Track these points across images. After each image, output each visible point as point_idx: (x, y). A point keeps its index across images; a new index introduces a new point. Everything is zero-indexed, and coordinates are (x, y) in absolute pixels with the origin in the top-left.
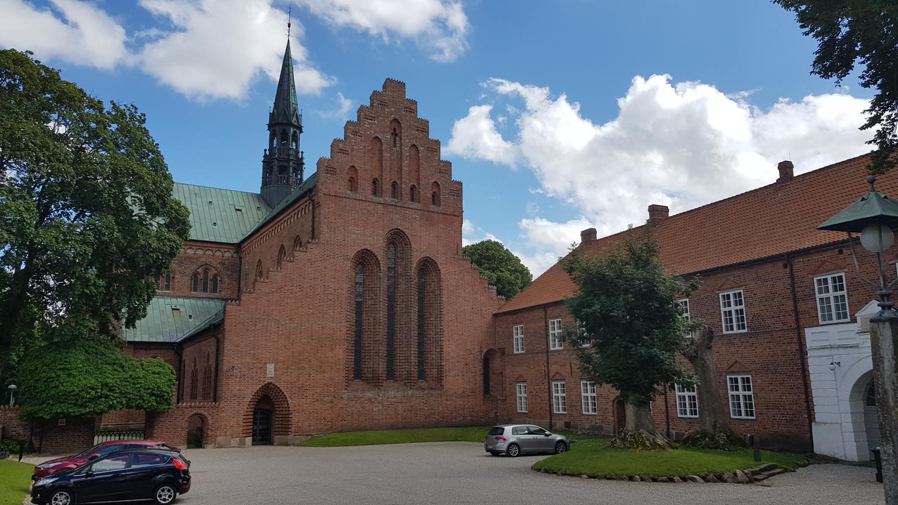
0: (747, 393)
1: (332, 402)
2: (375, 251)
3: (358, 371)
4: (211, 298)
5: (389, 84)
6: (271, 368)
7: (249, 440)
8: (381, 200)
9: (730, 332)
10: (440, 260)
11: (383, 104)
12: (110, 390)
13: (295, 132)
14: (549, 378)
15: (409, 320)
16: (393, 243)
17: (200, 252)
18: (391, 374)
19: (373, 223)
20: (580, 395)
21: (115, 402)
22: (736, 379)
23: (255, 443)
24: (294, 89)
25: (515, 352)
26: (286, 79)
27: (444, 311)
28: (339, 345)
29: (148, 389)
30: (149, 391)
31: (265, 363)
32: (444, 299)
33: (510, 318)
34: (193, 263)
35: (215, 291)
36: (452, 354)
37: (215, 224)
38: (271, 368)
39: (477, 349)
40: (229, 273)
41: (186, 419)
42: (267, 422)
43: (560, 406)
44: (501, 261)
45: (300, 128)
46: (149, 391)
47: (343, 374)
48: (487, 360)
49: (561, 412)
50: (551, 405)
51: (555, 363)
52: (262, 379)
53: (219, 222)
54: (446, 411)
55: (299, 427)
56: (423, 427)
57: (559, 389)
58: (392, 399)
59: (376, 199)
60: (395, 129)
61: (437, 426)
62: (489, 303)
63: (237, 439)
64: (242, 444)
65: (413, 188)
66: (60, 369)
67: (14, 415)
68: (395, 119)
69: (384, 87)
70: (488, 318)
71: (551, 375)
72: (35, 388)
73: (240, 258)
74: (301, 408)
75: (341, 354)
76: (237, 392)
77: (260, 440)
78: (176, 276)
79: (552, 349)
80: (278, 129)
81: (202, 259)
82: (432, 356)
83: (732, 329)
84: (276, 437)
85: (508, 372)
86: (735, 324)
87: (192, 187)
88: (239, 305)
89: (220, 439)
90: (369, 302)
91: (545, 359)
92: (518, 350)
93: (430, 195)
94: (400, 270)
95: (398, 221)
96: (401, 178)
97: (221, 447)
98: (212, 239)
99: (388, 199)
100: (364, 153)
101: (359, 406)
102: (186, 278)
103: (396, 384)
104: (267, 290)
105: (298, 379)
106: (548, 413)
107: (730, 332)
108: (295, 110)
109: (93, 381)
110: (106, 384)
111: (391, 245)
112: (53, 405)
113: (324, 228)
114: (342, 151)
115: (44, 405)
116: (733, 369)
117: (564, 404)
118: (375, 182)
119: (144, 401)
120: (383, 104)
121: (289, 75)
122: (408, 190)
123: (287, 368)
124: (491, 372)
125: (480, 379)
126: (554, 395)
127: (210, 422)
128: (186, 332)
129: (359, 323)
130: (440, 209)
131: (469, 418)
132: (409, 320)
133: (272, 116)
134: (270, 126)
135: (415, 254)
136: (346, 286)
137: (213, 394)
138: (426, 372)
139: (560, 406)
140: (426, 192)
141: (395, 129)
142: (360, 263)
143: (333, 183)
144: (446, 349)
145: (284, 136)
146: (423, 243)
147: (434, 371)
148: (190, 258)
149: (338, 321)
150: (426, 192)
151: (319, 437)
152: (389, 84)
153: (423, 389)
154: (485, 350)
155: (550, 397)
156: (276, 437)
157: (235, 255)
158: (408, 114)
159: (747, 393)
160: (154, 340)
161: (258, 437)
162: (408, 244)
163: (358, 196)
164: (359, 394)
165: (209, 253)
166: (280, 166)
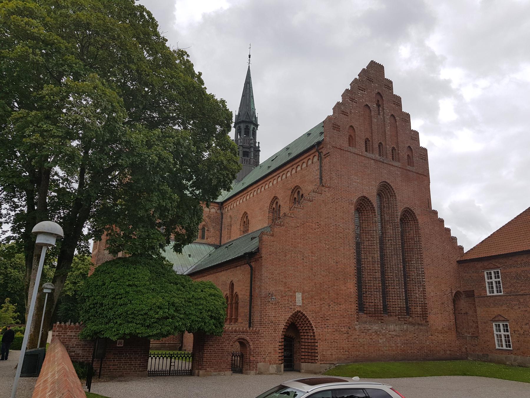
0: (506, 333)
4: (201, 243)
5: (373, 64)
9: (492, 294)
10: (417, 212)
11: (370, 80)
12: (176, 310)
13: (254, 128)
15: (395, 262)
21: (180, 323)
22: (499, 325)
24: (253, 99)
26: (248, 92)
27: (424, 256)
30: (210, 313)
31: (295, 292)
33: (479, 265)
35: (203, 237)
36: (432, 294)
39: (449, 290)
40: (214, 224)
42: (296, 347)
45: (257, 126)
52: (293, 307)
55: (323, 356)
58: (390, 334)
60: (378, 101)
61: (426, 359)
63: (275, 366)
66: (129, 285)
67: (73, 334)
68: (379, 93)
72: (102, 304)
73: (222, 214)
76: (273, 319)
80: (243, 126)
82: (417, 294)
83: (493, 293)
84: (303, 365)
86: (495, 289)
89: (260, 365)
90: (366, 243)
94: (387, 218)
97: (260, 373)
100: (359, 116)
103: (391, 319)
107: (492, 294)
108: (254, 113)
109: (161, 300)
110: (173, 304)
112: (120, 324)
115: (111, 324)
116: (497, 319)
119: (205, 323)
121: (250, 89)
123: (312, 297)
128: (189, 267)
129: (359, 261)
131: (448, 352)
132: (395, 262)
135: (399, 204)
138: (412, 311)
140: (403, 154)
141: (378, 101)
145: (247, 133)
146: (404, 196)
147: (419, 309)
150: (403, 154)
152: (373, 64)
156: (303, 365)
157: (219, 212)
158: (387, 90)
159: (506, 333)
162: (394, 195)
164: (368, 326)
166: (244, 152)
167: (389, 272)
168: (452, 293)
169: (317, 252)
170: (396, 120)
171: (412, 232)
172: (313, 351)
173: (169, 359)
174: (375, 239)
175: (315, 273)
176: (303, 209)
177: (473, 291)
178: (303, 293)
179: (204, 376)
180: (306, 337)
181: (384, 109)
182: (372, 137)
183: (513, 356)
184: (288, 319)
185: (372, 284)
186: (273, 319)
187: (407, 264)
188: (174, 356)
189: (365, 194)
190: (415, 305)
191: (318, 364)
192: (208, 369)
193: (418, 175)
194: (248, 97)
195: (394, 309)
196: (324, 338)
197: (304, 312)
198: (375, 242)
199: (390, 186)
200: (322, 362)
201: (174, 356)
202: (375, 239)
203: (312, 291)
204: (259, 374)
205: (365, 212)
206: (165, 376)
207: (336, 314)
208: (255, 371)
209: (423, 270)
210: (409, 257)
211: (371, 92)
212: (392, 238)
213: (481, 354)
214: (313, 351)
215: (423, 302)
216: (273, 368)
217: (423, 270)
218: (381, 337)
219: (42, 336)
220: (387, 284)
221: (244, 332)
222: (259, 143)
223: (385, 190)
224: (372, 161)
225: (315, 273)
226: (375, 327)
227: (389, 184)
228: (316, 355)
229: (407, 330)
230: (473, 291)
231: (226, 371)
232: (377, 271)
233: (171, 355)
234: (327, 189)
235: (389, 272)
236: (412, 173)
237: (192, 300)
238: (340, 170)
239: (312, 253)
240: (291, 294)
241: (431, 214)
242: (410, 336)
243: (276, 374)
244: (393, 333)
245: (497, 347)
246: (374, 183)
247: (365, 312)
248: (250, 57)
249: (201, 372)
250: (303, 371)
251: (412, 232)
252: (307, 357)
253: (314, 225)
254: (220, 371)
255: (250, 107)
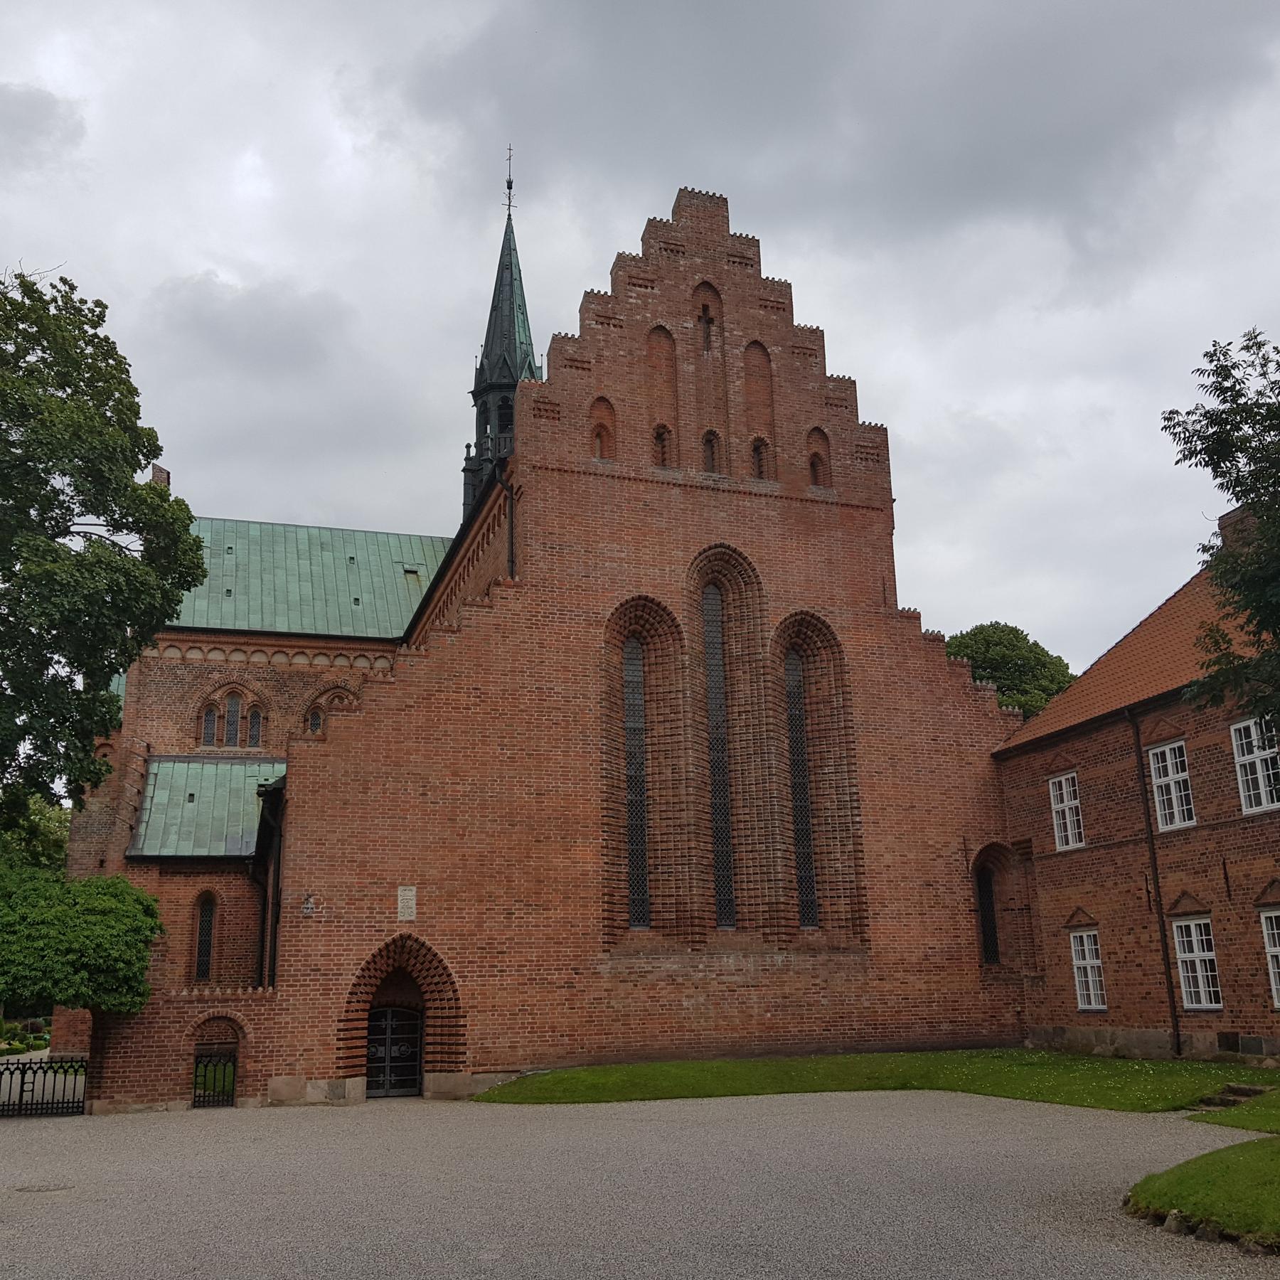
1: (570, 985)
2: (666, 601)
3: (636, 904)
6: (407, 898)
7: (357, 1085)
8: (679, 476)
10: (838, 620)
11: (674, 250)
14: (1162, 911)
15: (763, 774)
16: (716, 583)
17: (321, 661)
18: (726, 910)
19: (660, 533)
20: (1261, 953)
23: (374, 1089)
24: (524, 313)
25: (1060, 848)
27: (860, 749)
28: (585, 836)
29: (69, 951)
30: (71, 957)
31: (394, 886)
32: (857, 716)
33: (1038, 761)
34: (306, 684)
36: (888, 859)
37: (357, 600)
38: (407, 898)
39: (955, 844)
41: (189, 1030)
43: (1202, 988)
44: (1022, 670)
46: (71, 957)
47: (596, 911)
48: (986, 870)
49: (1205, 1004)
50: (1172, 987)
51: (1178, 866)
52: (385, 926)
53: (365, 598)
54: (879, 1008)
55: (486, 1051)
56: (820, 1051)
57: (1195, 938)
58: (733, 979)
59: (661, 474)
61: (857, 1047)
62: (983, 726)
64: (336, 1097)
65: (758, 447)
69: (676, 211)
70: (982, 765)
71: (1166, 902)
74: (489, 1004)
75: (588, 859)
77: (393, 1086)
78: (271, 715)
79: (1163, 828)
80: (493, 399)
81: (328, 677)
82: (836, 863)
85: (1045, 902)
87: (315, 532)
88: (323, 740)
89: (276, 1083)
90: (660, 730)
91: (1146, 859)
92: (1067, 840)
93: (802, 462)
94: (736, 648)
95: (722, 526)
96: (727, 423)
97: (278, 1103)
98: (348, 631)
99: (695, 474)
100: (630, 365)
101: (643, 997)
102: (293, 719)
103: (743, 938)
104: (393, 703)
105: (480, 925)
106: (1166, 1008)
111: (711, 589)
113: (535, 549)
114: (574, 363)
116: (1074, 922)
117: (1212, 981)
118: (661, 434)
120: (674, 250)
121: (511, 285)
122: (746, 450)
123: (451, 895)
124: (998, 907)
125: (968, 926)
126: (1181, 956)
127: (251, 1037)
130: (832, 495)
131: (945, 1027)
133: (480, 372)
134: (476, 394)
136: (595, 687)
137: (263, 969)
138: (815, 905)
139: (1202, 988)
142: (634, 634)
143: (554, 440)
144: (871, 846)
146: (791, 576)
147: (843, 906)
148: (301, 674)
149: (578, 777)
150: (794, 455)
151: (530, 1085)
153: (813, 950)
154: (976, 848)
155: (1169, 964)
156: (429, 1079)
158: (737, 268)
160: (203, 852)
161: (387, 1078)
163: (618, 469)
164: (641, 963)
165: (341, 662)
167: (741, 804)
168: (966, 851)
169: (473, 772)
170: (768, 355)
171: (825, 681)
172: (453, 1040)
173: (17, 1074)
174: (681, 716)
175: (464, 829)
176: (426, 657)
177: (1030, 840)
178: (422, 885)
179: (106, 1112)
180: (438, 1004)
181: (722, 329)
182: (676, 419)
183: (1110, 1029)
184: (368, 958)
185: (671, 845)
186: (322, 961)
187: (813, 778)
188: (30, 1068)
189: (647, 591)
190: (833, 893)
191: (465, 1074)
192: (117, 1097)
193: (846, 510)
194: (506, 312)
195: (753, 908)
196: (489, 1002)
197: (422, 939)
198: (681, 724)
199: (740, 554)
200: (481, 1069)
201: (30, 1068)
202: (681, 716)
203: (452, 878)
204: (272, 1105)
205: (656, 639)
206: (12, 1116)
207: (530, 935)
208: (259, 1098)
209: (854, 790)
210: (817, 756)
211: (676, 286)
212: (749, 708)
213: (1050, 1028)
214: (453, 1040)
215: (854, 885)
216: (317, 1089)
217: (854, 790)
218: (691, 991)
219: (1268, 980)
220: (736, 841)
221: (227, 1001)
222: (1253, 343)
223: (722, 571)
224: (676, 491)
225: (464, 829)
226: (670, 965)
227: (735, 551)
228: (462, 1049)
229: (786, 968)
230: (1030, 840)
231: (171, 1099)
232: (684, 806)
233: (24, 1065)
234: (511, 592)
235: (741, 804)
236: (823, 507)
237: (17, 927)
238: (557, 530)
239: (455, 774)
240: (379, 891)
241: (893, 623)
242: (798, 985)
243: (326, 1104)
244: (735, 978)
245: (1187, 1005)
246: (681, 554)
247: (653, 923)
248: (510, 187)
249: (97, 1104)
250: (427, 1094)
251: (825, 681)
252: (439, 1057)
253: (463, 698)
254: (153, 1100)
255: (512, 339)
